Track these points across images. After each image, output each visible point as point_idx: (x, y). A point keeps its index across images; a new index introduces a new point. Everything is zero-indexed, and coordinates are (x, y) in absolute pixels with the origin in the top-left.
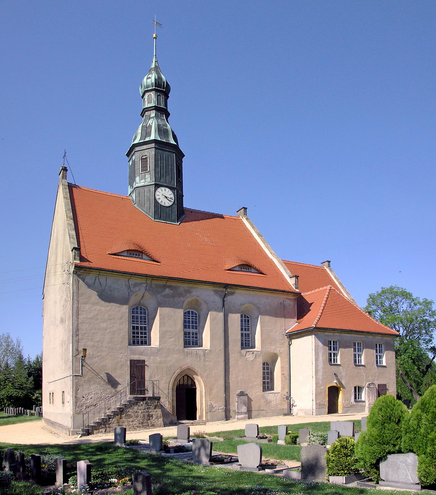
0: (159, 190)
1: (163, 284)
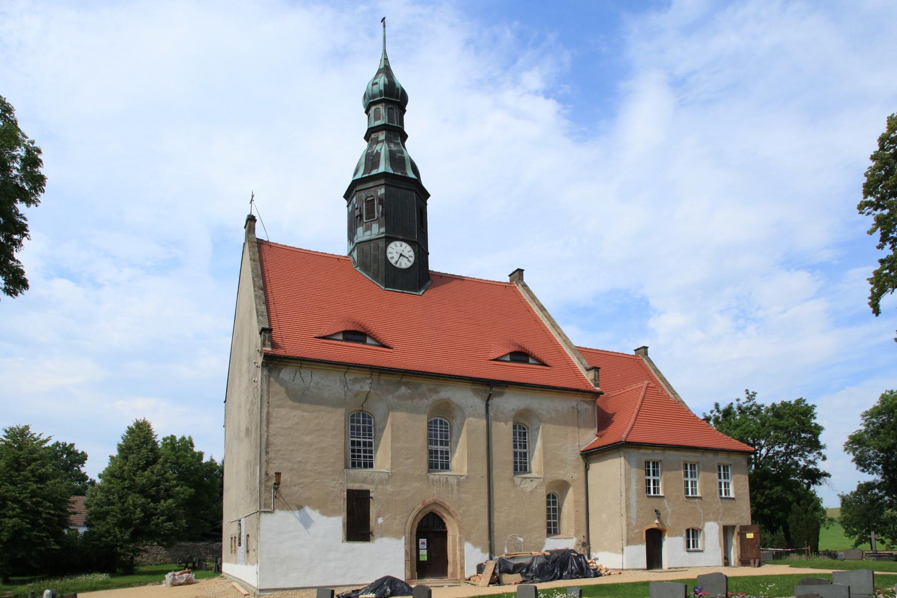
0: (392, 245)
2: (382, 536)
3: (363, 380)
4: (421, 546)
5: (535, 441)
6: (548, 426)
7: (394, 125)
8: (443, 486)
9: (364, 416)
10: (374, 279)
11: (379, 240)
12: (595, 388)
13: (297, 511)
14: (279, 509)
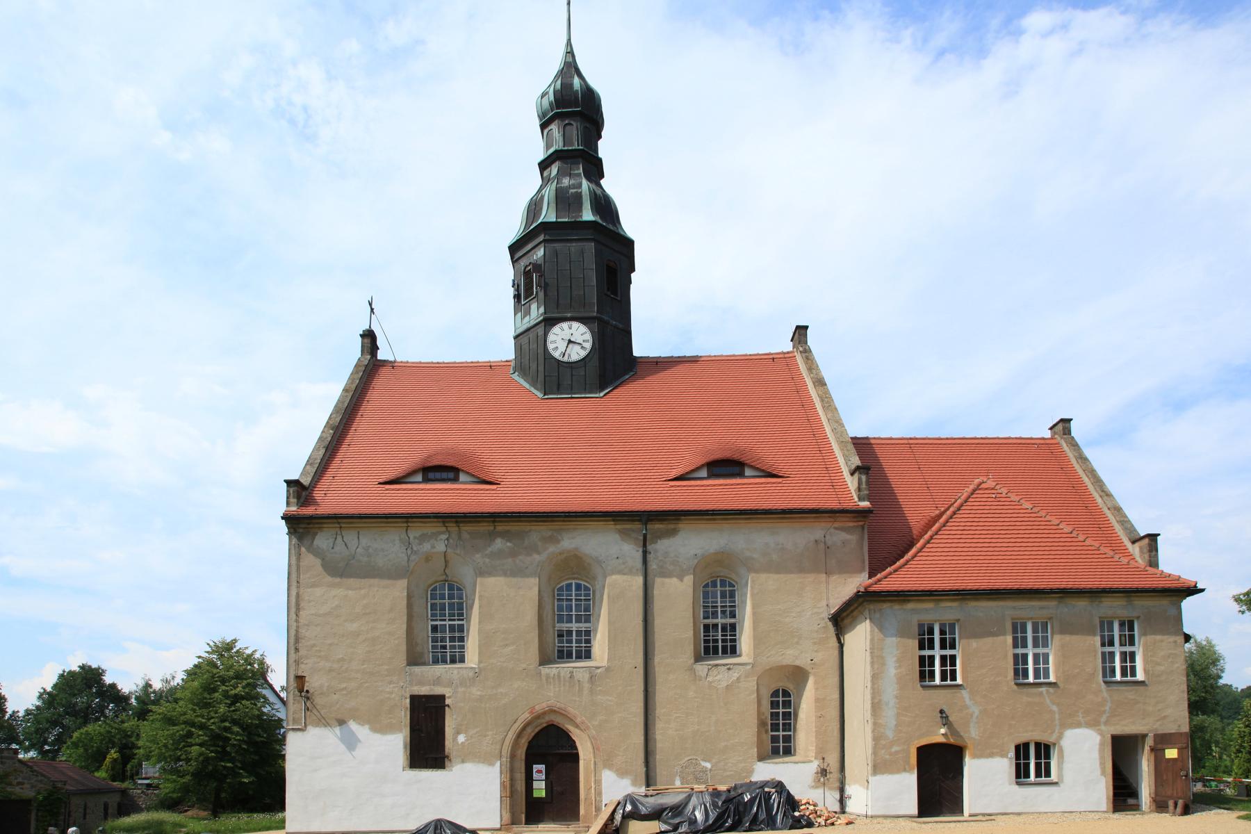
0: (556, 329)
1: (489, 530)
2: (463, 762)
3: (435, 536)
4: (535, 775)
5: (744, 602)
6: (763, 576)
7: (574, 148)
8: (564, 685)
9: (451, 588)
11: (538, 327)
12: (860, 503)
13: (338, 728)
14: (312, 726)
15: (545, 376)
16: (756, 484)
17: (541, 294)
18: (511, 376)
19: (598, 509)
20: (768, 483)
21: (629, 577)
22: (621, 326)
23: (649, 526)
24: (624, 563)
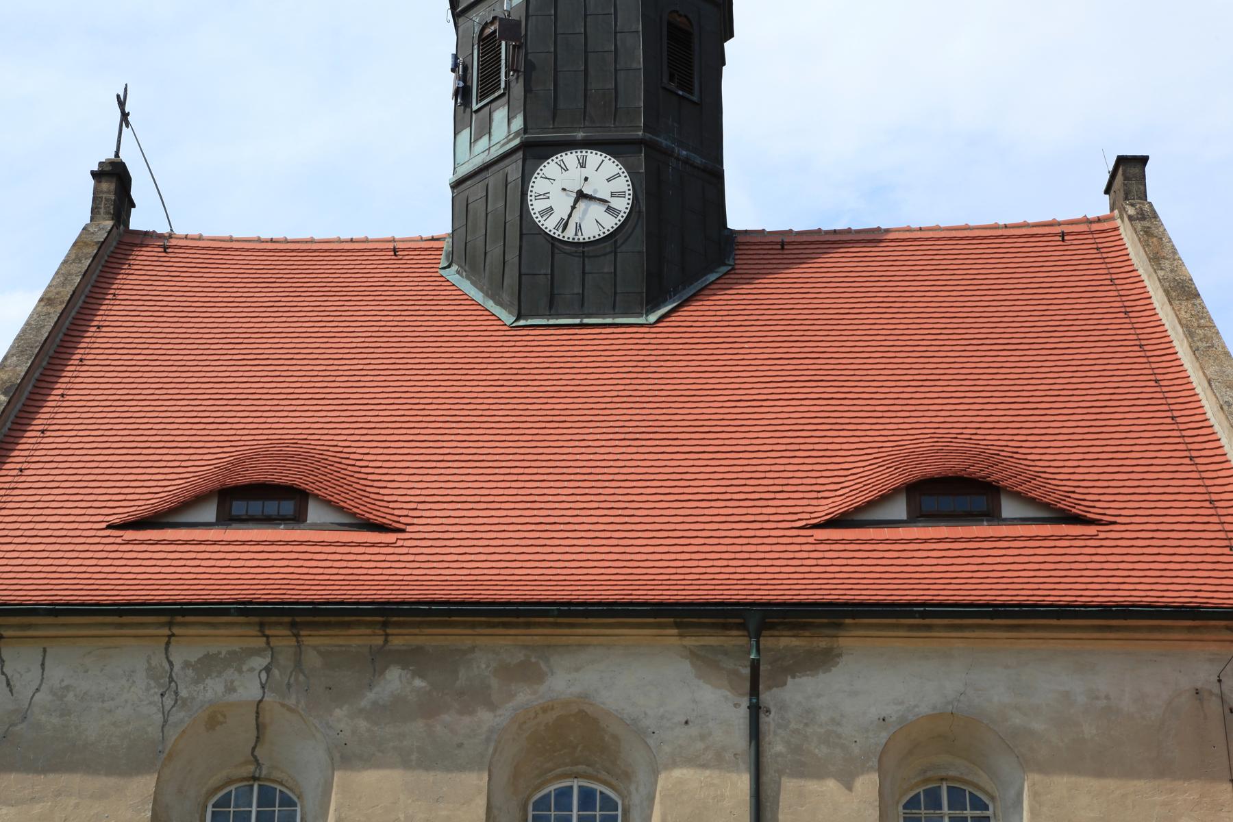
0: (550, 167)
3: (236, 659)
6: (1061, 783)
9: (266, 798)
10: (492, 297)
11: (507, 161)
15: (520, 275)
16: (1031, 538)
17: (518, 89)
18: (442, 272)
19: (640, 595)
20: (1061, 538)
21: (716, 773)
22: (698, 160)
23: (764, 642)
24: (702, 737)
